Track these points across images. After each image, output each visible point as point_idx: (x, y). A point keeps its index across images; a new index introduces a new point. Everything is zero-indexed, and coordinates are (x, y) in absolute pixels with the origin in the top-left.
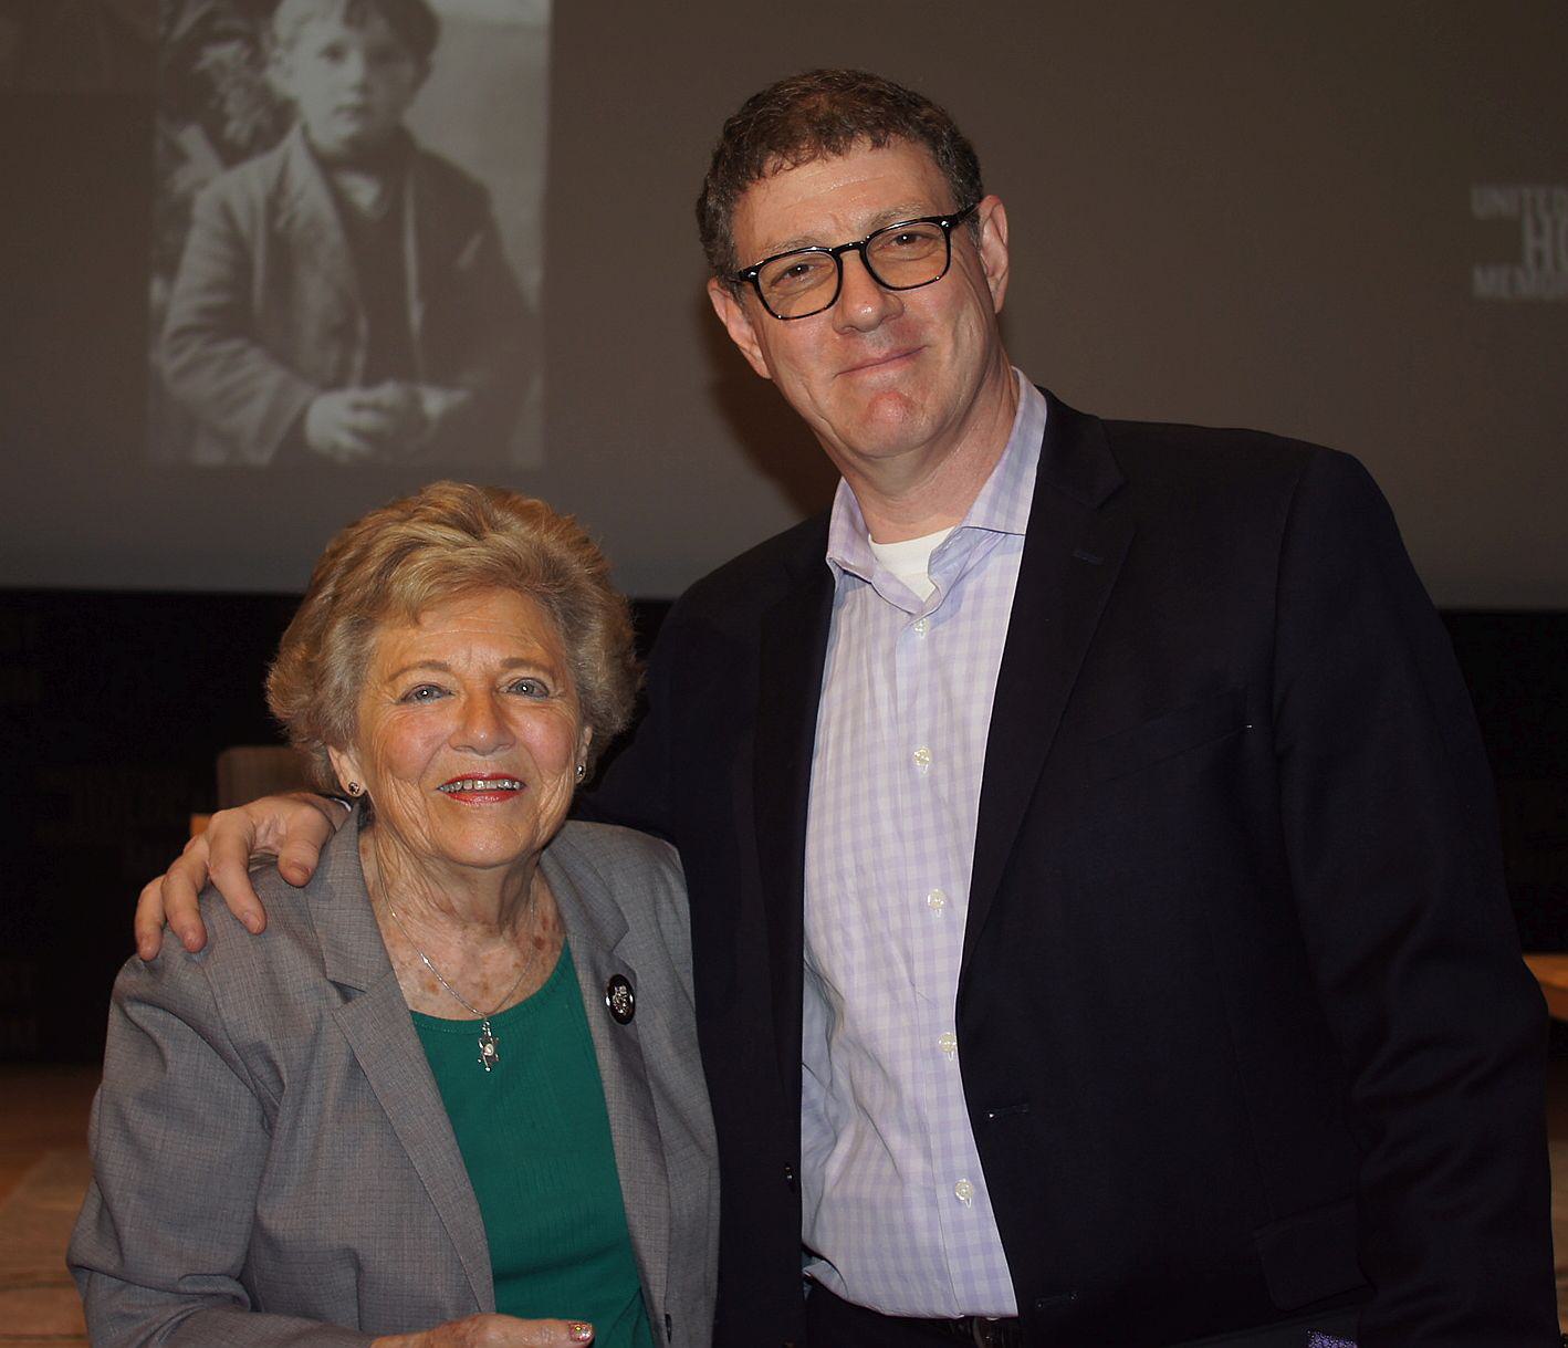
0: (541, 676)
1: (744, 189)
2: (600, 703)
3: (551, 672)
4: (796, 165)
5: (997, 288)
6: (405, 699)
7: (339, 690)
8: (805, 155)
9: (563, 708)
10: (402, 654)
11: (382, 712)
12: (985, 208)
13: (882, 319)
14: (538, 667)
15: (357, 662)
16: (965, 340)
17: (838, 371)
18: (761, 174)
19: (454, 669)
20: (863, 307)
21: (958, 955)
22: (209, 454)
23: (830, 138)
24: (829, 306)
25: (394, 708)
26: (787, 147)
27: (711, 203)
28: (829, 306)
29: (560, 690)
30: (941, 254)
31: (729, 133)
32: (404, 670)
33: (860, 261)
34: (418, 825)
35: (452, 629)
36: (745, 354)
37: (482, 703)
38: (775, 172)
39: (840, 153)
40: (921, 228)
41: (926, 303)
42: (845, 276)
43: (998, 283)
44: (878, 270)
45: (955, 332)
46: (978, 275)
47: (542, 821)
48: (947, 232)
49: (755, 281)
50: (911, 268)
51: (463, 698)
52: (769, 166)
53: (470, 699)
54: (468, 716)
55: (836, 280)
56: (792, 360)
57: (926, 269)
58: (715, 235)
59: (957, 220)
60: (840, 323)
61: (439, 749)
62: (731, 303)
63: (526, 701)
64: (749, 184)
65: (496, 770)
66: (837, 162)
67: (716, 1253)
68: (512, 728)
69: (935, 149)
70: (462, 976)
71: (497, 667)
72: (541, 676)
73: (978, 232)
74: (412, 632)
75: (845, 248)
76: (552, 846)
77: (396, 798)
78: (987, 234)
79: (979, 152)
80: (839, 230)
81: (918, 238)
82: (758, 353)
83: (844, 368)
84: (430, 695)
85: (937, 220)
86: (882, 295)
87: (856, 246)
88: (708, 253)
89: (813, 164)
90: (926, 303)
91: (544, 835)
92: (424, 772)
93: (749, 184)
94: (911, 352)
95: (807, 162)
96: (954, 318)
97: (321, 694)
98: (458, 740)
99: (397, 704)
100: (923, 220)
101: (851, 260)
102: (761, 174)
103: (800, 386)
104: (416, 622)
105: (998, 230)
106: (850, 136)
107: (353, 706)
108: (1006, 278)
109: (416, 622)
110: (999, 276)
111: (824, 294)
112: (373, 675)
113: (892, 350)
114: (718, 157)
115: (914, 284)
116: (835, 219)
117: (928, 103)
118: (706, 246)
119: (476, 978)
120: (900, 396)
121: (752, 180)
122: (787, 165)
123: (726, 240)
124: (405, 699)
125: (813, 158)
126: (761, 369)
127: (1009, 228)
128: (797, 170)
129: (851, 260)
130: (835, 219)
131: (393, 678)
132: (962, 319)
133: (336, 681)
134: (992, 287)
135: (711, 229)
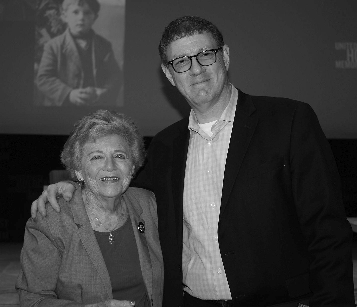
0: (123, 154)
1: (169, 43)
2: (137, 160)
3: (125, 153)
4: (181, 38)
5: (227, 66)
6: (92, 159)
7: (77, 157)
8: (183, 35)
9: (128, 161)
10: (92, 149)
11: (87, 162)
12: (224, 47)
13: (201, 73)
14: (123, 152)
15: (81, 151)
16: (220, 77)
17: (191, 84)
18: (173, 40)
19: (103, 152)
23: (189, 31)
24: (189, 70)
25: (90, 161)
26: (179, 33)
28: (189, 70)
29: (128, 157)
30: (214, 58)
32: (92, 153)
33: (196, 60)
34: (95, 188)
35: (103, 143)
36: (170, 81)
37: (110, 160)
38: (176, 39)
39: (191, 35)
40: (210, 52)
41: (211, 69)
42: (192, 63)
43: (227, 64)
44: (200, 62)
46: (223, 63)
48: (216, 53)
50: (208, 61)
51: (105, 159)
52: (175, 38)
53: (107, 159)
54: (106, 163)
56: (180, 82)
57: (211, 61)
58: (163, 54)
59: (218, 50)
60: (191, 73)
61: (100, 171)
62: (166, 69)
64: (170, 42)
66: (191, 37)
68: (117, 166)
69: (213, 34)
70: (105, 222)
71: (113, 152)
72: (123, 154)
73: (223, 53)
74: (94, 144)
75: (192, 56)
77: (90, 182)
78: (225, 53)
79: (223, 35)
80: (191, 52)
81: (209, 54)
82: (173, 80)
83: (192, 84)
84: (98, 158)
85: (213, 50)
86: (201, 67)
87: (195, 56)
88: (161, 58)
89: (185, 37)
90: (211, 69)
92: (97, 176)
93: (170, 42)
94: (207, 80)
95: (184, 37)
96: (217, 72)
98: (104, 169)
99: (90, 160)
100: (210, 50)
101: (194, 59)
102: (173, 40)
103: (182, 88)
104: (95, 142)
106: (194, 31)
107: (80, 161)
108: (229, 63)
109: (95, 142)
110: (227, 63)
111: (188, 67)
112: (85, 154)
113: (203, 80)
114: (164, 36)
115: (208, 65)
116: (190, 50)
117: (211, 24)
118: (161, 56)
119: (108, 223)
120: (205, 90)
121: (171, 41)
122: (179, 38)
123: (165, 55)
124: (92, 159)
125: (185, 36)
126: (173, 84)
127: (230, 52)
129: (194, 59)
130: (190, 50)
131: (90, 154)
133: (76, 155)
134: (226, 65)
135: (162, 52)
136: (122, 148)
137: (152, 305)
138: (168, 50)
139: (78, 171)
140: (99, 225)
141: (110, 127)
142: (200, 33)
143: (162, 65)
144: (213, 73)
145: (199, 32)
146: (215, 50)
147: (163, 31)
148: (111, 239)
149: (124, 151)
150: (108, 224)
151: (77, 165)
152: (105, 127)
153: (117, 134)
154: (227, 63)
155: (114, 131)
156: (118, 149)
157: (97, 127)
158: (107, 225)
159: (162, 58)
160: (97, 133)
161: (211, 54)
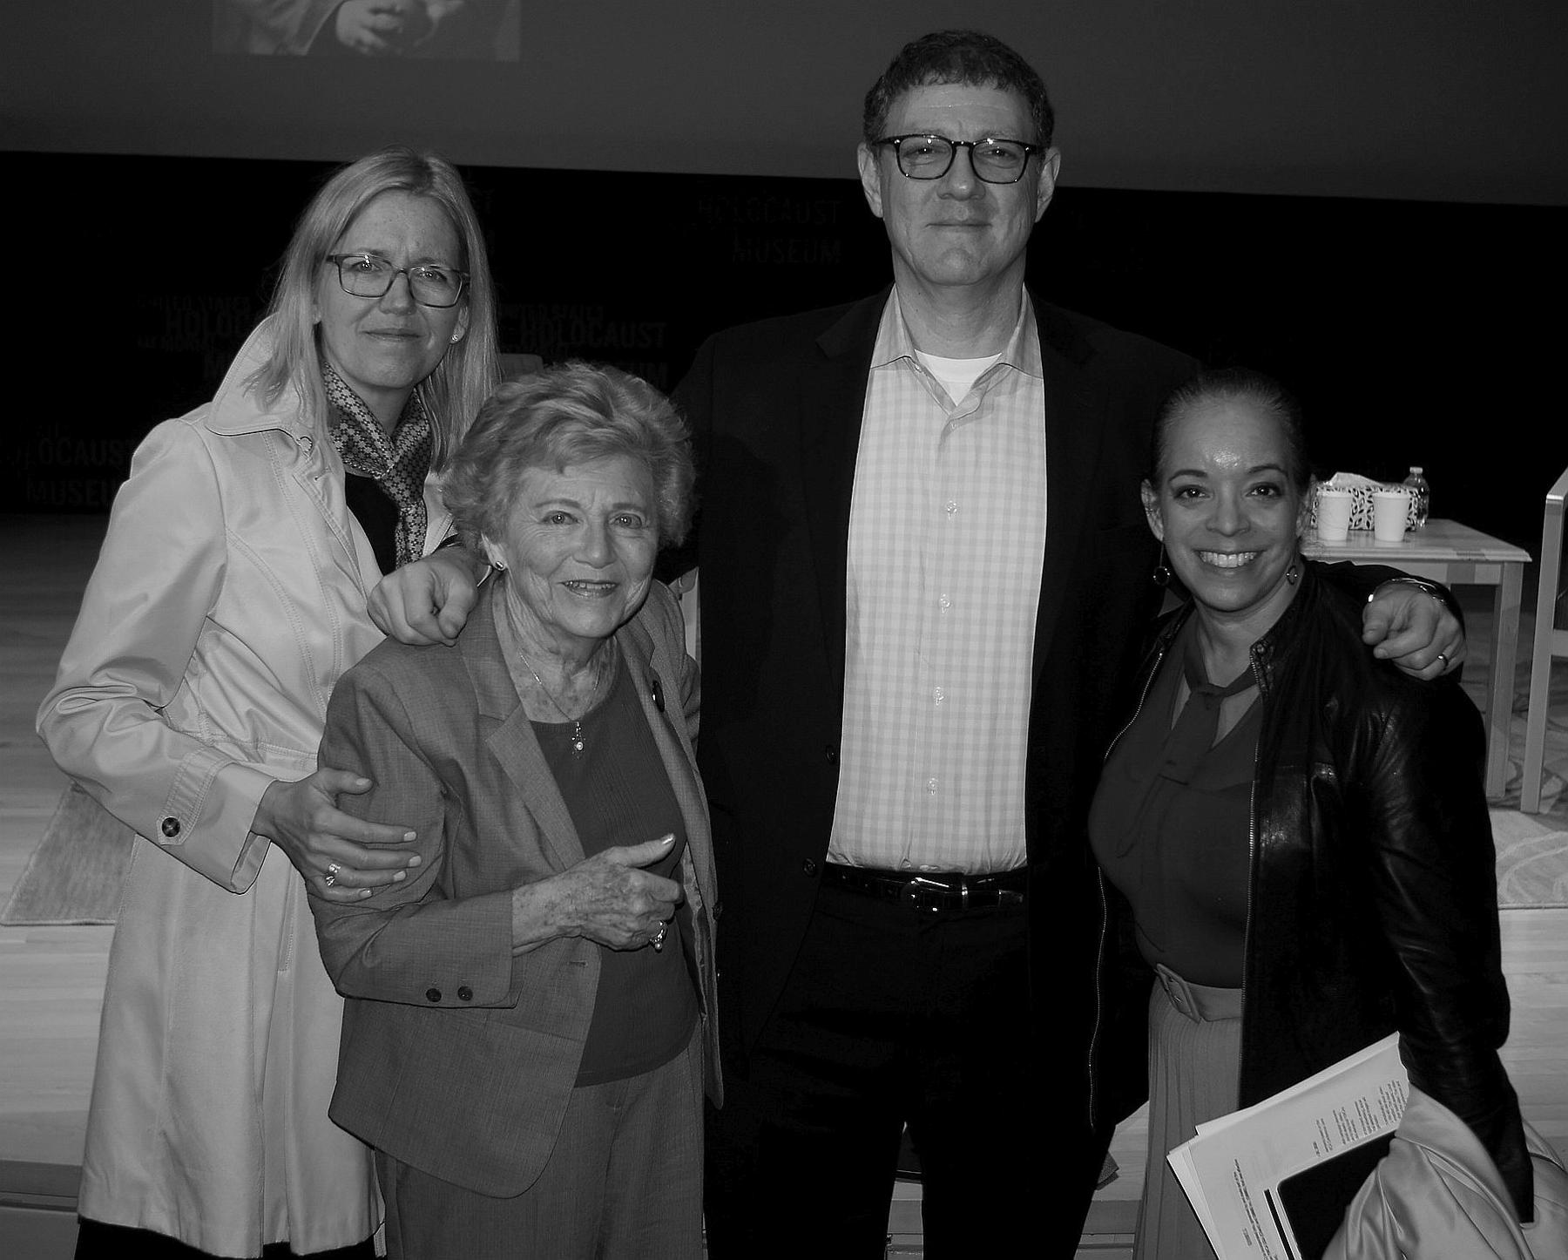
0: (638, 514)
1: (906, 88)
2: (670, 529)
3: (645, 512)
4: (946, 82)
5: (1041, 206)
6: (546, 521)
7: (500, 504)
9: (650, 536)
12: (1051, 153)
13: (969, 197)
14: (637, 509)
15: (514, 490)
16: (1015, 231)
17: (930, 221)
18: (921, 82)
19: (582, 507)
20: (961, 185)
21: (1039, 563)
22: (261, 47)
23: (972, 72)
24: (937, 178)
25: (537, 527)
26: (944, 70)
27: (880, 93)
28: (937, 178)
30: (1018, 171)
31: (907, 51)
32: (548, 502)
34: (545, 604)
36: (868, 197)
38: (930, 83)
40: (1012, 148)
41: (1001, 195)
42: (955, 161)
43: (1042, 205)
44: (977, 165)
45: (1011, 222)
46: (1032, 192)
47: (627, 608)
48: (1027, 154)
49: (897, 146)
50: (995, 169)
51: (586, 526)
52: (928, 78)
53: (591, 528)
54: (589, 540)
55: (949, 162)
56: (904, 207)
57: (1007, 175)
58: (875, 115)
59: (1034, 151)
60: (944, 190)
61: (566, 559)
62: (871, 161)
63: (628, 532)
64: (910, 86)
65: (603, 578)
66: (972, 89)
67: (668, 769)
69: (1033, 103)
70: (562, 694)
71: (610, 508)
72: (638, 514)
73: (1041, 168)
74: (556, 477)
75: (959, 144)
76: (630, 623)
78: (1045, 172)
79: (1057, 118)
80: (961, 132)
81: (1006, 155)
82: (878, 199)
83: (934, 221)
85: (1024, 145)
86: (976, 181)
87: (967, 144)
88: (866, 125)
89: (957, 85)
91: (626, 616)
92: (554, 572)
93: (910, 86)
94: (979, 225)
95: (953, 82)
96: (1013, 214)
97: (486, 506)
98: (580, 556)
99: (539, 523)
101: (962, 153)
102: (921, 82)
103: (903, 225)
104: (561, 471)
105: (1053, 170)
106: (985, 75)
107: (506, 516)
108: (1048, 202)
109: (561, 471)
110: (1044, 199)
112: (524, 498)
113: (970, 218)
114: (894, 65)
116: (960, 125)
117: (1036, 76)
118: (867, 121)
119: (571, 694)
120: (965, 252)
121: (914, 84)
122: (940, 80)
123: (882, 119)
124: (546, 521)
125: (958, 82)
126: (877, 209)
128: (944, 86)
129: (962, 153)
130: (960, 125)
131: (540, 505)
132: (1018, 217)
133: (499, 497)
134: (1039, 205)
135: (873, 109)
136: (636, 498)
137: (146, 702)
138: (894, 108)
139: (495, 541)
140: (546, 703)
141: (612, 436)
142: (1000, 86)
143: (863, 146)
144: (1002, 211)
145: (999, 84)
146: (1027, 145)
147: (894, 51)
148: (579, 746)
149: (641, 506)
150: (570, 698)
151: (495, 524)
152: (596, 433)
153: (628, 452)
154: (1044, 199)
155: (623, 444)
156: (624, 500)
157: (571, 430)
158: (566, 699)
159: (867, 127)
160: (571, 451)
161: (1013, 156)
